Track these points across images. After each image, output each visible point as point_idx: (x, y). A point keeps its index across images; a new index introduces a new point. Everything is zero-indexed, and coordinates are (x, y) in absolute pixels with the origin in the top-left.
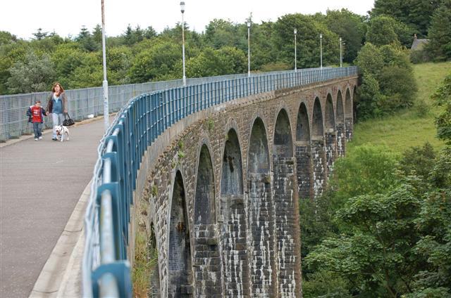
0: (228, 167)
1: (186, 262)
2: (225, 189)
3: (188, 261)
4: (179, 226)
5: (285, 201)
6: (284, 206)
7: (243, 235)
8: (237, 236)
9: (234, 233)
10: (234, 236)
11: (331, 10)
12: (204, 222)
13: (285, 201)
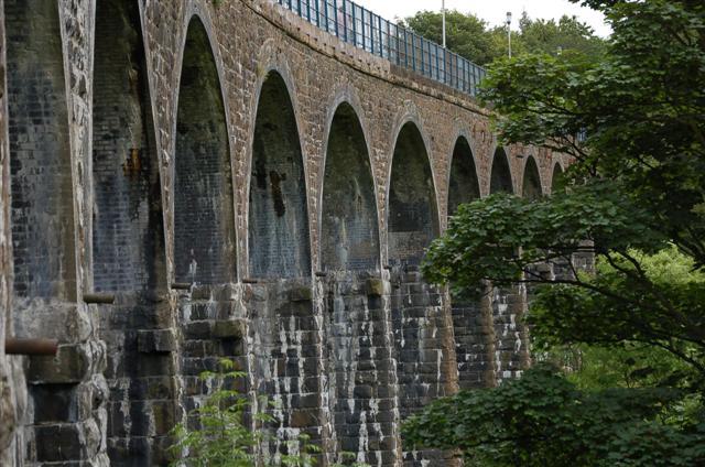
0: (271, 202)
1: (151, 268)
2: (262, 264)
3: (158, 263)
4: (130, 161)
5: (422, 380)
6: (421, 392)
7: (312, 385)
8: (294, 389)
9: (287, 382)
10: (287, 388)
11: (533, 18)
12: (204, 278)
13: (422, 380)
